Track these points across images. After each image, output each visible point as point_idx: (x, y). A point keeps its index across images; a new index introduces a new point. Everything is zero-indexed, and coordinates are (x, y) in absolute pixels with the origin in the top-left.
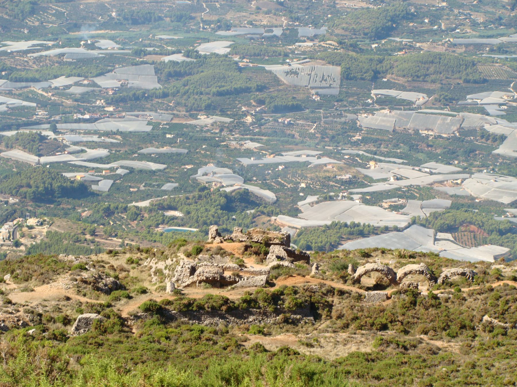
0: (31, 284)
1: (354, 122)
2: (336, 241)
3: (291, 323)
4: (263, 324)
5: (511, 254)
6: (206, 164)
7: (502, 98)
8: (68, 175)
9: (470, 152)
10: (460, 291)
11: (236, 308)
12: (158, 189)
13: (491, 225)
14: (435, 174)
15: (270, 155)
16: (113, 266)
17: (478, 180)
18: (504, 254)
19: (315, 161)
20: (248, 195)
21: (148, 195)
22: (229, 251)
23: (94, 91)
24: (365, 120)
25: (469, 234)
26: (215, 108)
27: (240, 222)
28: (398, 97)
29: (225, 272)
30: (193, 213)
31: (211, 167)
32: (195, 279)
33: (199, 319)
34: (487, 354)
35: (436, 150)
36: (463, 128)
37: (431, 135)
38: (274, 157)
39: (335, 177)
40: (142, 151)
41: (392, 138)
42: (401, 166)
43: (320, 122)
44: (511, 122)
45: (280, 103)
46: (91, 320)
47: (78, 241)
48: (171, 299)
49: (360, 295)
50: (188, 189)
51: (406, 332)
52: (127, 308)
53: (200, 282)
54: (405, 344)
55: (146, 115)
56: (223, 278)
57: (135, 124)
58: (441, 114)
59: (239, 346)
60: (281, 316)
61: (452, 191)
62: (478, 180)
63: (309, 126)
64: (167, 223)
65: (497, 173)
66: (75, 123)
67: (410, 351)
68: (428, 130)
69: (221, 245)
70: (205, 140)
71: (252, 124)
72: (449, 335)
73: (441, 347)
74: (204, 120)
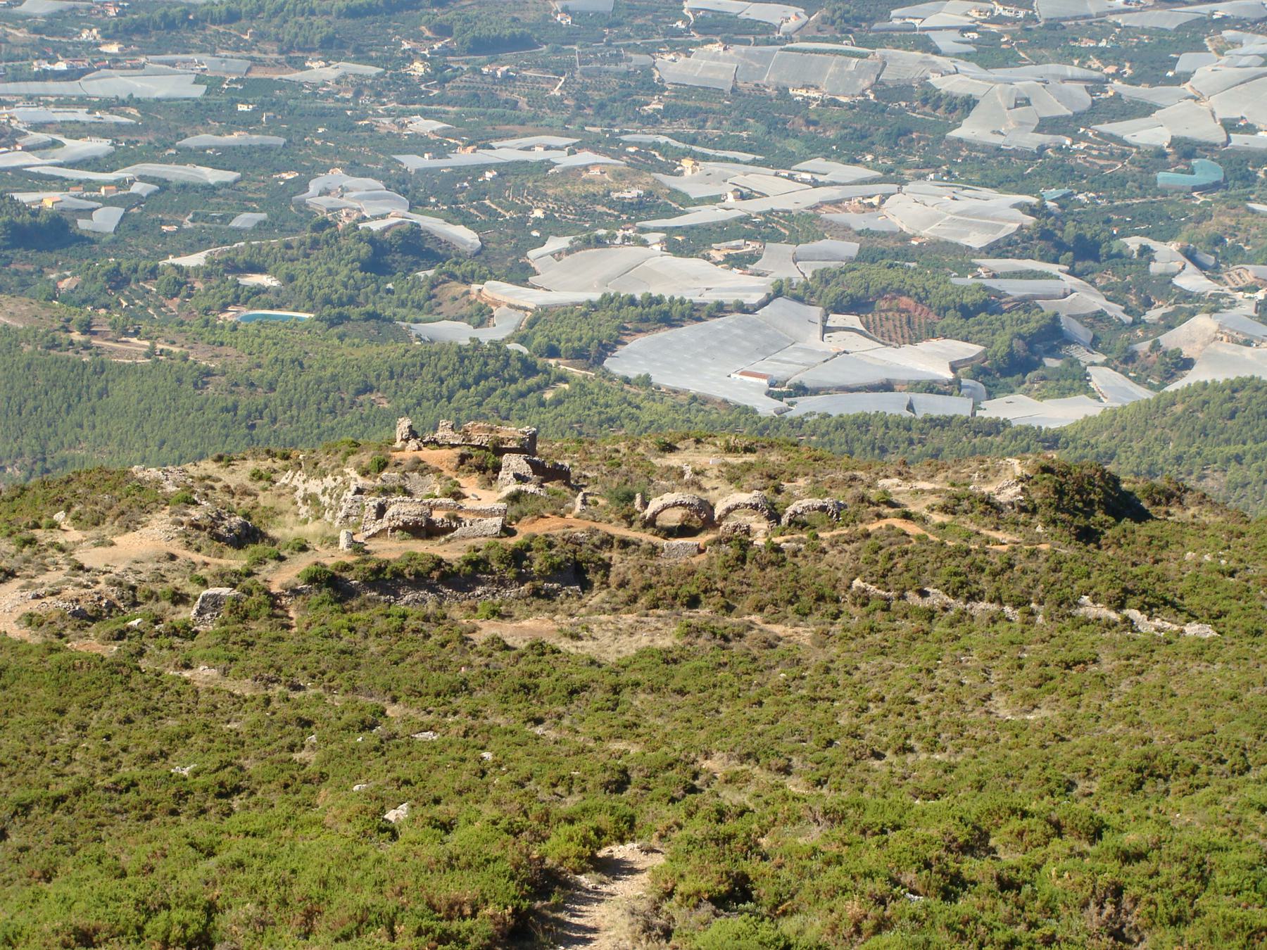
0: (107, 530)
1: (647, 71)
2: (611, 336)
3: (543, 597)
4: (498, 598)
5: (986, 359)
6: (326, 170)
7: (967, 15)
8: (25, 198)
9: (899, 136)
10: (816, 537)
11: (456, 574)
12: (223, 226)
13: (944, 296)
14: (823, 184)
15: (465, 147)
16: (228, 487)
17: (917, 197)
18: (972, 359)
19: (564, 160)
20: (419, 237)
21: (200, 240)
22: (433, 463)
23: (74, 8)
24: (672, 67)
25: (897, 315)
26: (342, 45)
27: (404, 296)
28: (743, 16)
29: (434, 512)
30: (301, 279)
31: (336, 176)
32: (386, 524)
33: (396, 595)
34: (853, 646)
35: (825, 131)
36: (882, 83)
37: (815, 99)
38: (474, 151)
39: (608, 195)
40: (185, 142)
41: (730, 107)
42: (750, 168)
43: (573, 72)
44: (986, 68)
45: (485, 32)
46: (222, 598)
47: (54, 345)
48: (349, 560)
49: (655, 548)
50: (288, 226)
51: (729, 609)
52: (280, 578)
53: (394, 530)
54: (726, 632)
55: (192, 61)
56: (430, 523)
57: (167, 81)
58: (836, 52)
59: (464, 640)
60: (527, 586)
61: (859, 222)
62: (917, 197)
63: (548, 81)
64: (245, 303)
65: (957, 180)
66: (36, 80)
67: (732, 644)
68: (807, 87)
69: (419, 454)
70: (323, 115)
71: (425, 78)
72: (797, 611)
73: (781, 635)
74: (319, 71)
